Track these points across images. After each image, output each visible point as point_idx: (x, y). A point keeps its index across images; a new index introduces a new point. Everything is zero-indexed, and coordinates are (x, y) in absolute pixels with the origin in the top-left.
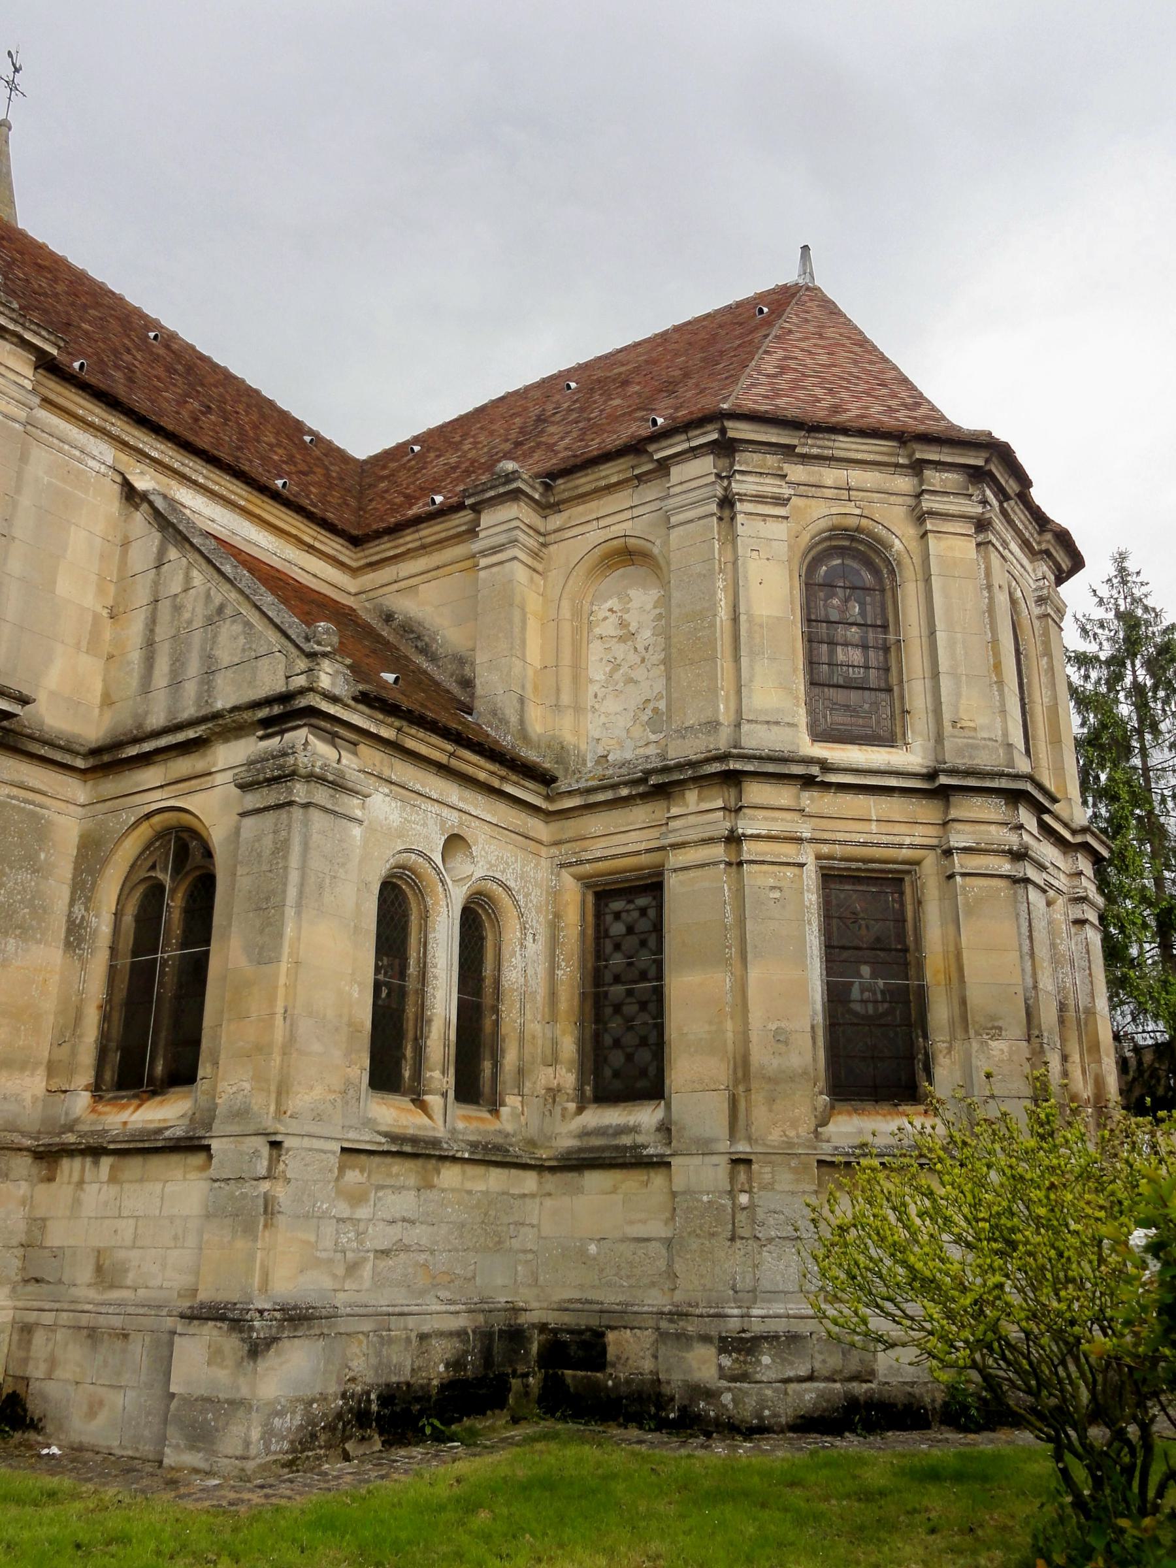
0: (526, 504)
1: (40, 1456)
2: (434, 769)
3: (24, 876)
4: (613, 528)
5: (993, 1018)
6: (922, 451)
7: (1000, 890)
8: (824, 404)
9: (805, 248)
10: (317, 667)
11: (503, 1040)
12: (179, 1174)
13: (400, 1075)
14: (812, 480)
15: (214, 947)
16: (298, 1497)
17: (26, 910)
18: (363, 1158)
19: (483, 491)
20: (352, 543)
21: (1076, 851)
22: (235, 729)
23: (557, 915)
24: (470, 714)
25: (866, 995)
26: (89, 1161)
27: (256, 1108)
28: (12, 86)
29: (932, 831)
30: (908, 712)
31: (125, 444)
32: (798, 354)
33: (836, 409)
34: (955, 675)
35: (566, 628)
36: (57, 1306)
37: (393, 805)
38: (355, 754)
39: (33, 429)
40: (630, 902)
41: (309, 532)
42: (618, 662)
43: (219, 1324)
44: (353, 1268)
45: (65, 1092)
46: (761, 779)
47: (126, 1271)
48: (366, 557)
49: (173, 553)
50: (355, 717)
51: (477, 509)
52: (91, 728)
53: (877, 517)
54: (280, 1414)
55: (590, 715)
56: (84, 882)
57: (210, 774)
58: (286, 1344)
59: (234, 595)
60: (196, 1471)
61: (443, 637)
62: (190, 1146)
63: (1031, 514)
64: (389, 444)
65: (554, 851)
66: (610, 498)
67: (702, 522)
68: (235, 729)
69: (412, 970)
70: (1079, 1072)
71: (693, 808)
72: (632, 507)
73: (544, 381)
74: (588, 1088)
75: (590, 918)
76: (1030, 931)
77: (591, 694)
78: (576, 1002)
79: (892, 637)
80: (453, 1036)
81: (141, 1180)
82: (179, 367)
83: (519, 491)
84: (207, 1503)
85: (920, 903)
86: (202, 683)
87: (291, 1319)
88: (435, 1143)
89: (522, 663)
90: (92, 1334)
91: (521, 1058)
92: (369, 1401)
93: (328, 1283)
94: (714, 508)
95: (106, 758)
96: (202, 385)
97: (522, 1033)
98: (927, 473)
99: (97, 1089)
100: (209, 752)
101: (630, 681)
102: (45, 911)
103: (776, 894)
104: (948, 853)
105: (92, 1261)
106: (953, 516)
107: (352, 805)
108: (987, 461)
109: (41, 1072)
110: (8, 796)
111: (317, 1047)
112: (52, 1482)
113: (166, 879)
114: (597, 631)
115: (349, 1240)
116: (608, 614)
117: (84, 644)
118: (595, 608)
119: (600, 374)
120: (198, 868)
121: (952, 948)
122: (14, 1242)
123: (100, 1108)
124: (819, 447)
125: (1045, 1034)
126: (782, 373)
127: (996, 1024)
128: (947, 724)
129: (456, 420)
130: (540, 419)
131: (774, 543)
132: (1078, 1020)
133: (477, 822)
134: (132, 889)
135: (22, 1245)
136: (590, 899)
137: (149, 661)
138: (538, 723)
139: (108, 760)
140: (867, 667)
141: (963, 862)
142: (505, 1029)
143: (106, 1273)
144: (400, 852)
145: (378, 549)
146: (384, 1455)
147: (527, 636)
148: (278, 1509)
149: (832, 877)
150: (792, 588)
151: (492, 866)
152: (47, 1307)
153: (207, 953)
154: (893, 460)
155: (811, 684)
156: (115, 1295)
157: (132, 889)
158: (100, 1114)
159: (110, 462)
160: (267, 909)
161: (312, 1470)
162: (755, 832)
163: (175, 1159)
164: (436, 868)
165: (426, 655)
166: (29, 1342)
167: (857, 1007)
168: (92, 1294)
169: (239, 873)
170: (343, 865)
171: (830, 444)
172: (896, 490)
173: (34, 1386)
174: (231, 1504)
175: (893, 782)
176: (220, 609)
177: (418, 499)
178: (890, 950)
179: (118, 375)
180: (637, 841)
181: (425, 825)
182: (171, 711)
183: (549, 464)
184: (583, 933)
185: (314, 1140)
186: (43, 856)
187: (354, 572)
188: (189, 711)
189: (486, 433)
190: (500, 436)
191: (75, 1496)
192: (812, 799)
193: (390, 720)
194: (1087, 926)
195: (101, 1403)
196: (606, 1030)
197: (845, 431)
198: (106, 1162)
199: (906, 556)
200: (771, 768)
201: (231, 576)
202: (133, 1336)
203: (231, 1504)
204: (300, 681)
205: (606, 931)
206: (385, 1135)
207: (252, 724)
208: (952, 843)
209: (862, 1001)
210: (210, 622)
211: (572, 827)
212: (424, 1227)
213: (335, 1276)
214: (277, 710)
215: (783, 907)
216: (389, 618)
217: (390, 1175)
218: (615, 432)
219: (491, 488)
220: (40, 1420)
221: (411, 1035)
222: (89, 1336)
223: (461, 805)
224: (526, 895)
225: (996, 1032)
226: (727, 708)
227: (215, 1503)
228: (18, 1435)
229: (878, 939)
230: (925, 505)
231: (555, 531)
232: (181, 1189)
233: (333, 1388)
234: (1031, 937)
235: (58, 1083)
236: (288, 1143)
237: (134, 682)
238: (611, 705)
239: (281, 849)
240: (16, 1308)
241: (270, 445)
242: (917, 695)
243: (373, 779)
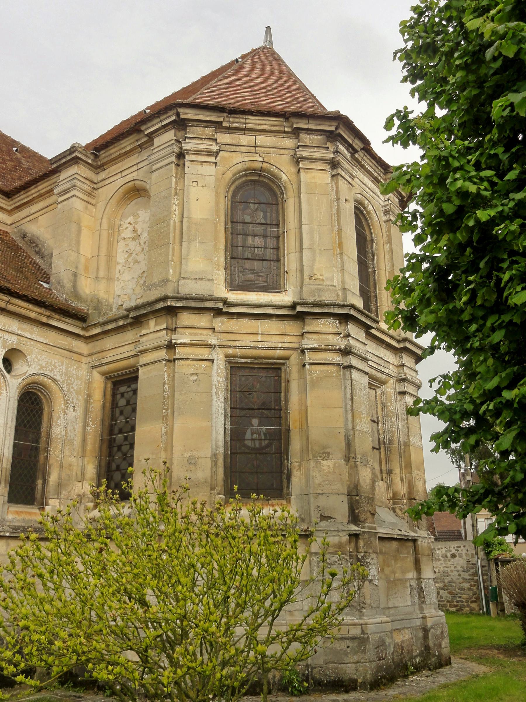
0: (84, 166)
4: (128, 176)
5: (325, 447)
6: (298, 123)
7: (333, 372)
8: (247, 101)
9: (268, 28)
11: (50, 467)
14: (234, 142)
20: (5, 196)
21: (402, 353)
23: (89, 396)
24: (48, 283)
25: (255, 436)
29: (295, 339)
30: (287, 272)
32: (244, 78)
33: (253, 103)
34: (312, 250)
35: (105, 234)
40: (129, 386)
46: (189, 311)
48: (14, 204)
53: (272, 162)
55: (116, 282)
61: (48, 244)
63: (377, 162)
65: (89, 359)
66: (128, 159)
67: (167, 167)
70: (399, 479)
71: (152, 330)
75: (109, 397)
76: (352, 396)
77: (117, 271)
78: (97, 445)
79: (281, 230)
83: (77, 158)
85: (288, 381)
89: (76, 254)
91: (60, 477)
94: (173, 159)
98: (302, 136)
101: (137, 262)
103: (195, 378)
104: (303, 351)
106: (316, 159)
108: (337, 128)
114: (123, 235)
118: (122, 223)
121: (303, 408)
124: (237, 123)
125: (359, 456)
126: (228, 87)
127: (326, 451)
128: (306, 277)
131: (207, 177)
132: (400, 449)
133: (32, 342)
136: (109, 386)
138: (87, 287)
140: (266, 248)
141: (310, 356)
145: (19, 199)
149: (237, 368)
150: (217, 203)
151: (42, 367)
153: (134, 434)
154: (282, 129)
155: (232, 258)
162: (183, 341)
167: (249, 443)
171: (243, 121)
172: (284, 147)
175: (270, 311)
178: (271, 409)
180: (128, 351)
184: (104, 406)
187: (10, 212)
192: (223, 323)
194: (407, 395)
196: (113, 460)
197: (251, 113)
199: (289, 183)
200: (193, 304)
205: (117, 404)
208: (303, 346)
209: (252, 440)
211: (99, 345)
215: (198, 385)
216: (24, 236)
223: (20, 332)
225: (326, 455)
226: (174, 272)
229: (264, 404)
230: (299, 154)
231: (101, 181)
234: (352, 400)
238: (127, 276)
242: (291, 262)
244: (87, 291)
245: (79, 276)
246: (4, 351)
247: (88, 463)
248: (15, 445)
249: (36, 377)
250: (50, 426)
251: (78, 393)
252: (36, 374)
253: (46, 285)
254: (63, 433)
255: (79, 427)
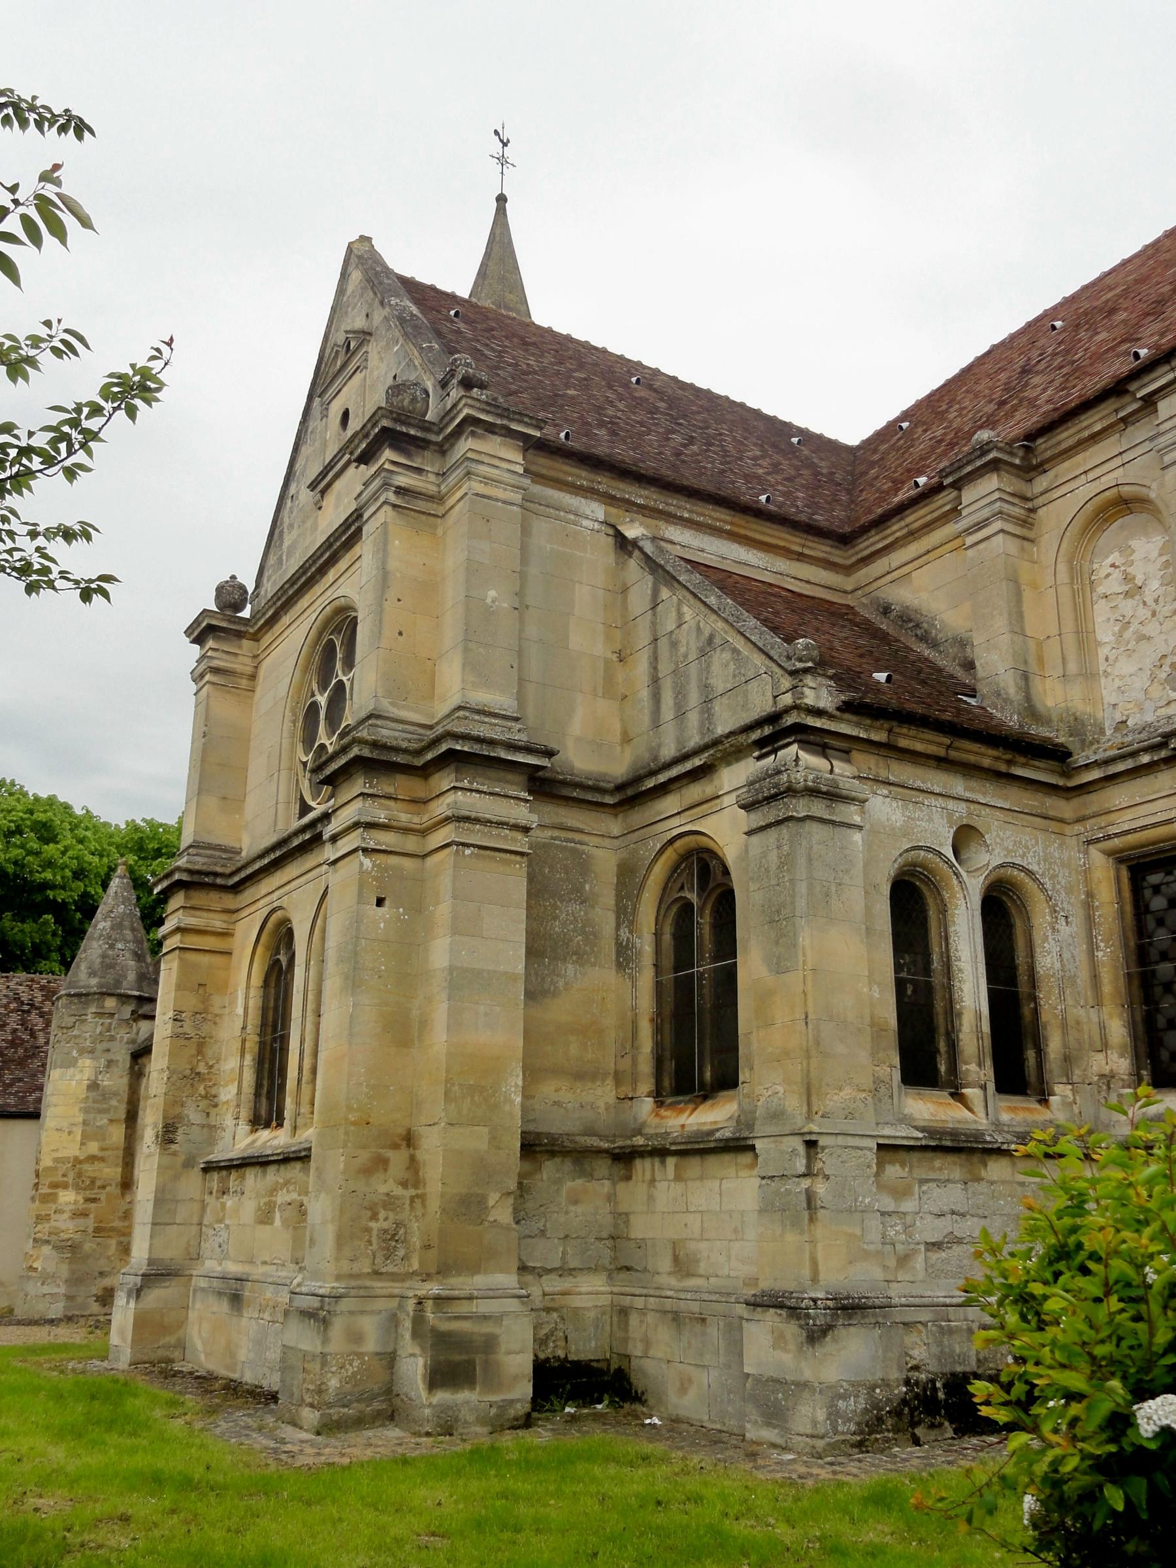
0: (1007, 472)
1: (643, 1425)
2: (933, 763)
3: (574, 907)
4: (1103, 479)
10: (800, 684)
11: (1045, 1028)
12: (732, 1171)
13: (936, 1070)
15: (740, 959)
16: (863, 1476)
17: (580, 938)
18: (902, 1155)
19: (960, 468)
22: (734, 753)
23: (1090, 895)
24: (974, 696)
26: (657, 1161)
27: (790, 1110)
28: (502, 161)
31: (613, 498)
36: (645, 1291)
37: (894, 804)
38: (849, 761)
39: (532, 505)
41: (795, 542)
42: (1127, 620)
43: (779, 1311)
44: (904, 1260)
45: (632, 1099)
47: (698, 1261)
49: (665, 593)
50: (843, 726)
51: (957, 485)
52: (618, 767)
54: (844, 1397)
55: (1103, 680)
56: (625, 907)
57: (718, 797)
58: (841, 1332)
59: (720, 624)
60: (774, 1446)
61: (942, 621)
62: (737, 1146)
64: (880, 424)
68: (734, 753)
69: (936, 964)
72: (1121, 453)
73: (1029, 325)
74: (1144, 1072)
75: (1127, 894)
78: (1122, 982)
80: (986, 1027)
81: (701, 1178)
82: (662, 405)
84: (779, 1475)
86: (702, 712)
87: (844, 1308)
88: (977, 1136)
90: (676, 1318)
91: (1065, 1045)
92: (935, 1390)
93: (878, 1274)
95: (630, 792)
96: (684, 416)
97: (1064, 1019)
99: (658, 1095)
100: (716, 776)
101: (1143, 638)
102: (595, 935)
105: (670, 1252)
107: (852, 814)
109: (610, 1081)
110: (552, 838)
111: (840, 1049)
112: (648, 1448)
113: (693, 897)
114: (1101, 590)
115: (897, 1232)
116: (1111, 570)
117: (600, 691)
118: (1095, 566)
119: (1086, 305)
120: (719, 885)
122: (605, 1235)
123: (663, 1112)
129: (944, 385)
130: (1025, 371)
134: (669, 908)
135: (613, 1238)
136: (1125, 874)
137: (656, 697)
138: (1053, 696)
139: (632, 794)
142: (1045, 1016)
143: (683, 1265)
144: (907, 851)
146: (955, 1442)
147: (1024, 609)
148: (840, 1485)
151: (1009, 851)
152: (637, 1293)
156: (692, 1283)
157: (669, 908)
158: (662, 1118)
159: (601, 518)
160: (779, 919)
161: (882, 1451)
163: (727, 1158)
164: (948, 862)
165: (926, 642)
166: (627, 1323)
168: (673, 1281)
169: (751, 889)
170: (847, 871)
173: (634, 1362)
174: (800, 1477)
176: (710, 640)
177: (903, 483)
179: (602, 433)
181: (930, 820)
182: (680, 741)
183: (1030, 423)
184: (1121, 911)
185: (849, 1138)
186: (587, 887)
188: (694, 740)
189: (971, 396)
190: (985, 396)
191: (664, 1460)
193: (878, 724)
195: (690, 1381)
196: (1158, 1010)
198: (671, 1161)
201: (715, 607)
202: (709, 1319)
203: (800, 1477)
204: (787, 700)
205: (1147, 907)
206: (922, 1129)
207: (749, 745)
210: (703, 653)
212: (975, 1219)
213: (885, 1268)
214: (767, 730)
216: (886, 610)
217: (933, 1169)
218: (1098, 374)
219: (969, 463)
220: (643, 1393)
221: (942, 1030)
222: (674, 1319)
223: (968, 795)
224: (1053, 877)
227: (787, 1475)
228: (627, 1406)
231: (1042, 494)
232: (735, 1189)
233: (895, 1375)
235: (626, 1090)
236: (823, 1141)
237: (646, 719)
238: (1125, 667)
239: (787, 862)
240: (612, 1293)
241: (754, 459)
243: (870, 783)
244: (1050, 703)
245: (1031, 677)
246: (952, 831)
247: (1111, 1018)
248: (990, 990)
249: (1002, 870)
250: (1031, 954)
251: (1069, 890)
252: (1002, 866)
253: (972, 701)
254: (1058, 965)
255: (1080, 951)
